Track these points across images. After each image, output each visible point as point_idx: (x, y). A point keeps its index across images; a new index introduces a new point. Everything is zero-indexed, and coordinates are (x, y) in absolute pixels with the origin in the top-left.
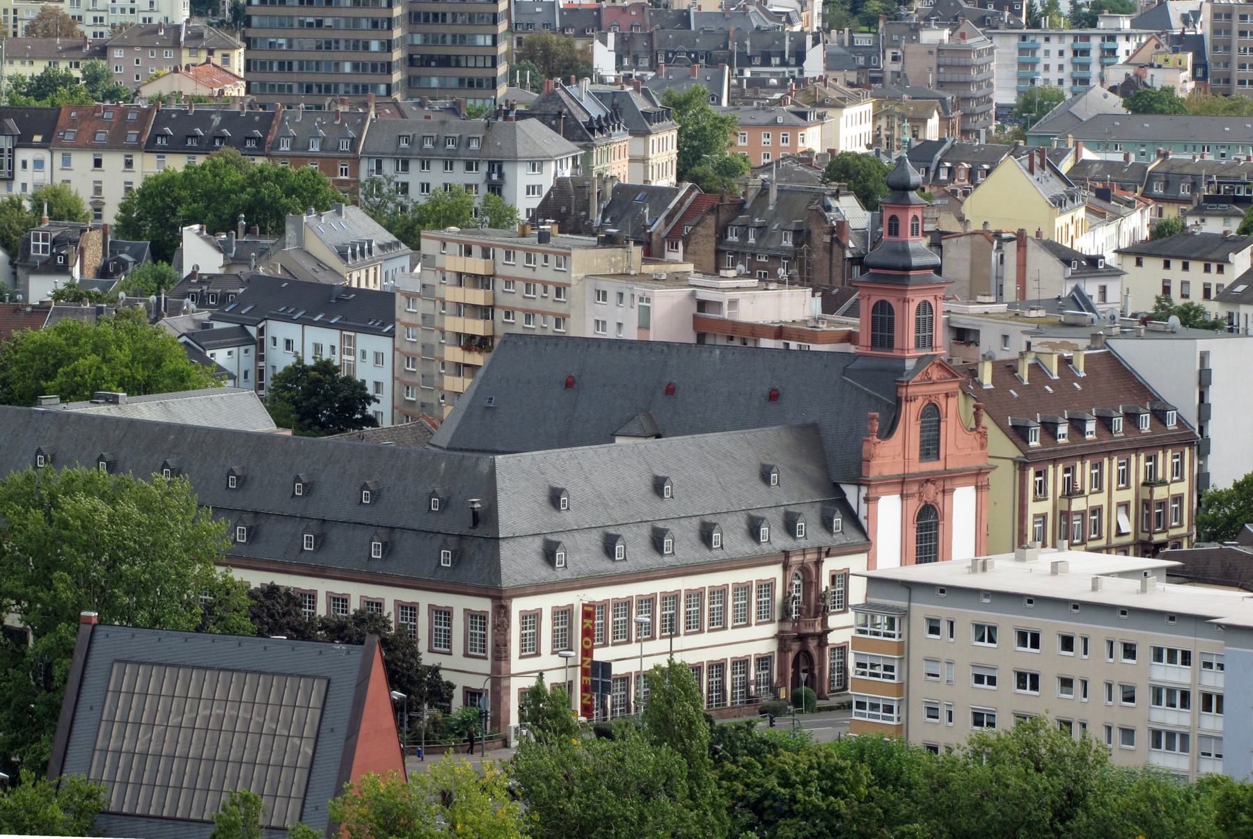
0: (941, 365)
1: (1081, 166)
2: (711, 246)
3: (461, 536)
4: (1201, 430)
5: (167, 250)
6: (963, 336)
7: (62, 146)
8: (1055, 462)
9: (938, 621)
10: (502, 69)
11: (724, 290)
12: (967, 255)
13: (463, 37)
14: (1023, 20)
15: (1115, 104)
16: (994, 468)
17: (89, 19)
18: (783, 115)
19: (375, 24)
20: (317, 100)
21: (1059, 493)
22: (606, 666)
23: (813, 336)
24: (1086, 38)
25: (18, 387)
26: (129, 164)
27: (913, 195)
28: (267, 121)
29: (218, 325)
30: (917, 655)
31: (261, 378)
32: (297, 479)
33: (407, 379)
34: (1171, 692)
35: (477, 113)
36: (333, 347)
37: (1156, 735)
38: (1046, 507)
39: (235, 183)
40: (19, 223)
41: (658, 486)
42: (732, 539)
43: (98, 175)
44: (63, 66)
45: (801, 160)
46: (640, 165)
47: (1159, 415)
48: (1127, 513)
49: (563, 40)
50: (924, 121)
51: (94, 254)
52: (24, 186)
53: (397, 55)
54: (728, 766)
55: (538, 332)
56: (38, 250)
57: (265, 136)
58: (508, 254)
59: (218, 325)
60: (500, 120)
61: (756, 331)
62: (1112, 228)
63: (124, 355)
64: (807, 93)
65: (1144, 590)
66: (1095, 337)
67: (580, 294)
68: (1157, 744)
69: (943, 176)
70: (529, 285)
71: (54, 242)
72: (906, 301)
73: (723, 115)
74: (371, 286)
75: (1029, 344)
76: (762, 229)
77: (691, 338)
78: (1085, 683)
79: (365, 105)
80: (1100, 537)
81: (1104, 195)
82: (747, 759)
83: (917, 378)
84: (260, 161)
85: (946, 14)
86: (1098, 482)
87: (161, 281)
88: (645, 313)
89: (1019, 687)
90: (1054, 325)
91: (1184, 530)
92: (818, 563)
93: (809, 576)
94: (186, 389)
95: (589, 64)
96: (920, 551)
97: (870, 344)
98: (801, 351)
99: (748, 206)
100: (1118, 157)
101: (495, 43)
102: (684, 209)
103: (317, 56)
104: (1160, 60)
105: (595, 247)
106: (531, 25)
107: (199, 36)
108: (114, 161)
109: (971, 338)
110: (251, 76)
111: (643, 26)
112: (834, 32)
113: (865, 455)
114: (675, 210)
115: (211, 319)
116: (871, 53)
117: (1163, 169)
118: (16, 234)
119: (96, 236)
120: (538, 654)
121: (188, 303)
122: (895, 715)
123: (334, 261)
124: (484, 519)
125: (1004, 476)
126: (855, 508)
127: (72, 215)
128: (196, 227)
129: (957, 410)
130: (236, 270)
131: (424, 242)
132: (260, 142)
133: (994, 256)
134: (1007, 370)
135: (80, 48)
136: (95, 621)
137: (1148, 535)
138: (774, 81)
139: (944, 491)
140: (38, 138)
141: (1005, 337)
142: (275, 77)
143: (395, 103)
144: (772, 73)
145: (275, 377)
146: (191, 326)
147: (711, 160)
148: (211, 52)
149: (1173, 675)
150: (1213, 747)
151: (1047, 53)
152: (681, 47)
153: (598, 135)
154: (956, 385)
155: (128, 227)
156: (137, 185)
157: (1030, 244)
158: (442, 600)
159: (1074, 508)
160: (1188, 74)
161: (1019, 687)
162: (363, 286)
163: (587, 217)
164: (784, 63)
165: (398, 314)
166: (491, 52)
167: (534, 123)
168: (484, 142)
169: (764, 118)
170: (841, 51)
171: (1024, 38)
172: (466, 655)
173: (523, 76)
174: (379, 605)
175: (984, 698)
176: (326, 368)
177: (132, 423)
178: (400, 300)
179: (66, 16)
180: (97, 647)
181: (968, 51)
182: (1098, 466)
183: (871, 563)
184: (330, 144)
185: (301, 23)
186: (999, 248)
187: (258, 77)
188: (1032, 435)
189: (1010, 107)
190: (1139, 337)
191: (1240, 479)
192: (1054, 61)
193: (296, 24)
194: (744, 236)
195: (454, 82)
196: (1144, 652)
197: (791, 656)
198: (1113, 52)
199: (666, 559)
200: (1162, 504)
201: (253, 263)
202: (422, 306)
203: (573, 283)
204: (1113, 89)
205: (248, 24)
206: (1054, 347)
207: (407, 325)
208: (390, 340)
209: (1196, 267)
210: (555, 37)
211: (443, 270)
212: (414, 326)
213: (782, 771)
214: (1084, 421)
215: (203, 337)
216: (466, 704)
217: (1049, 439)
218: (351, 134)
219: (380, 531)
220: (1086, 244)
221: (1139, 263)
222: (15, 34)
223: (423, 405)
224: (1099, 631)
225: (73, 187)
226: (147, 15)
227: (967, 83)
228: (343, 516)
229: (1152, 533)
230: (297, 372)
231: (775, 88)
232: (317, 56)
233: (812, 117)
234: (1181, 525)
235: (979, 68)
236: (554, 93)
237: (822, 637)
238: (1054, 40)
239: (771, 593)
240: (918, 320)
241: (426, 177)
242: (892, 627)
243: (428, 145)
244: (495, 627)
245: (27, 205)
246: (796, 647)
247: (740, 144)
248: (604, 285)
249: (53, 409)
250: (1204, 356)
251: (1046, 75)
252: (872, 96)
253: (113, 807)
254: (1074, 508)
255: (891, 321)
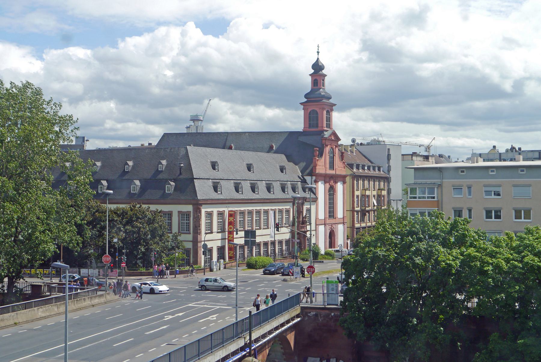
48: (375, 199)
97: (308, 127)
137: (380, 207)
244: (194, 218)
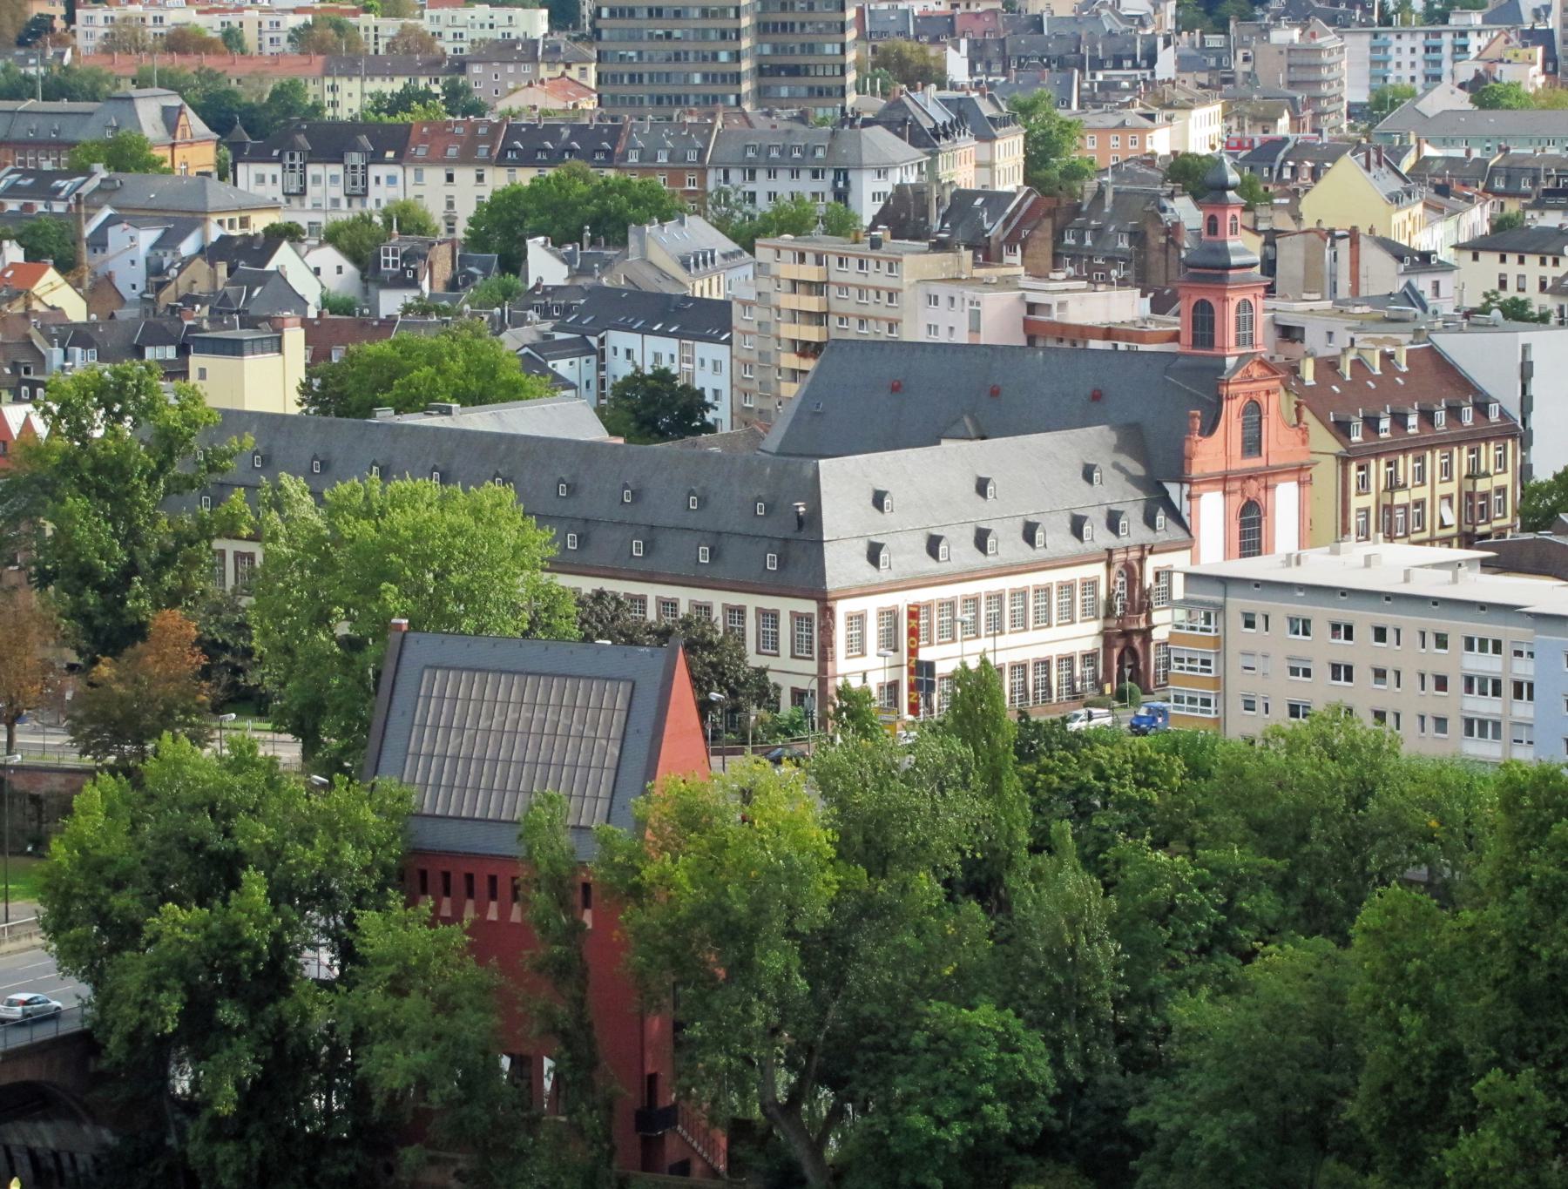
0: (1262, 363)
1: (1423, 163)
2: (1047, 248)
3: (786, 540)
4: (1524, 422)
5: (514, 262)
6: (1289, 333)
7: (413, 161)
8: (1377, 456)
9: (1253, 615)
10: (851, 77)
11: (1053, 292)
12: (1300, 252)
13: (811, 46)
14: (1376, 18)
15: (1462, 100)
16: (1316, 464)
17: (448, 34)
18: (1132, 116)
19: (723, 35)
20: (667, 112)
21: (1382, 486)
22: (930, 666)
23: (1141, 337)
24: (1438, 34)
25: (354, 400)
26: (480, 178)
27: (1231, 194)
28: (615, 133)
29: (559, 336)
30: (1233, 649)
31: (603, 387)
32: (626, 486)
33: (746, 386)
34: (1483, 681)
35: (823, 122)
36: (672, 356)
37: (1469, 723)
38: (1369, 501)
39: (581, 195)
40: (371, 238)
41: (982, 487)
42: (1056, 539)
43: (450, 190)
44: (422, 82)
45: (1144, 162)
46: (987, 170)
47: (1482, 408)
48: (1451, 505)
49: (916, 46)
50: (1275, 121)
51: (443, 267)
52: (378, 202)
53: (746, 65)
54: (1044, 760)
55: (872, 338)
56: (389, 262)
57: (614, 148)
58: (890, 266)
59: (559, 336)
60: (846, 128)
61: (1086, 332)
62: (1452, 222)
63: (458, 366)
64: (1156, 95)
65: (1455, 580)
66: (1417, 332)
67: (911, 298)
68: (1470, 732)
69: (1287, 175)
70: (862, 290)
71: (404, 257)
72: (1225, 300)
73: (1069, 119)
74: (715, 296)
75: (1352, 340)
76: (1099, 232)
77: (1022, 341)
78: (1398, 673)
79: (713, 115)
80: (1423, 530)
81: (1443, 190)
82: (1063, 753)
83: (1238, 376)
84: (611, 173)
85: (1298, 13)
86: (1421, 475)
87: (508, 293)
88: (975, 318)
89: (1334, 678)
90: (1378, 321)
91: (1508, 521)
92: (1141, 560)
93: (1132, 574)
94: (520, 399)
95: (943, 72)
96: (1243, 546)
98: (1129, 351)
99: (1085, 208)
100: (1461, 153)
101: (843, 51)
102: (1022, 213)
103: (667, 68)
104: (1509, 55)
105: (926, 252)
106: (885, 33)
107: (556, 50)
108: (465, 175)
109: (1297, 335)
110: (603, 88)
111: (996, 31)
112: (1185, 34)
113: (1186, 453)
114: (1013, 213)
115: (553, 329)
116: (1221, 54)
117: (1503, 164)
118: (368, 249)
119: (445, 250)
120: (863, 654)
121: (532, 315)
122: (1212, 708)
123: (679, 273)
124: (809, 527)
125: (1326, 472)
126: (1178, 505)
127: (421, 230)
128: (541, 239)
129: (1277, 406)
130: (581, 282)
131: (758, 250)
132: (609, 154)
133: (1328, 253)
134: (1329, 366)
135: (438, 63)
136: (405, 628)
138: (1125, 84)
139: (1266, 488)
140: (390, 154)
141: (1330, 334)
142: (626, 89)
143: (744, 114)
144: (1123, 76)
145: (614, 387)
146: (535, 338)
147: (1058, 163)
148: (568, 66)
149: (1485, 664)
150: (1524, 733)
151: (1399, 50)
152: (1034, 52)
153: (943, 141)
154: (1277, 383)
155: (477, 241)
156: (487, 199)
157: (1362, 240)
158: (769, 602)
159: (1396, 502)
160: (1538, 68)
161: (1334, 678)
162: (706, 296)
163: (926, 222)
164: (1136, 66)
165: (735, 322)
166: (840, 60)
167: (878, 130)
168: (830, 150)
169: (1112, 121)
170: (1193, 53)
171: (1376, 35)
172: (793, 656)
173: (873, 83)
174: (707, 609)
175: (1300, 690)
176: (663, 376)
177: (464, 434)
178: (736, 308)
179: (426, 32)
180: (407, 654)
181: (1318, 50)
182: (1422, 459)
183: (1195, 559)
184: (678, 154)
185: (651, 35)
186: (1333, 245)
187: (608, 91)
188: (1354, 431)
189: (1363, 105)
190: (1461, 331)
191: (1560, 470)
192: (1406, 58)
193: (646, 37)
194: (1081, 239)
195: (803, 91)
196: (1457, 642)
197: (1116, 652)
198: (1464, 48)
199: (989, 558)
200: (1485, 496)
201: (597, 274)
202: (758, 314)
203: (905, 288)
204: (1462, 86)
205: (599, 38)
206: (1377, 342)
207: (745, 333)
208: (726, 348)
209: (1532, 261)
210: (908, 45)
211: (777, 278)
212: (750, 333)
213: (1098, 765)
214: (1406, 416)
215: (547, 347)
216: (793, 703)
217: (1371, 434)
218: (699, 144)
219: (776, 543)
220: (1423, 241)
221: (1475, 258)
222: (376, 51)
223: (761, 412)
224: (1411, 622)
225: (426, 201)
226: (506, 30)
227: (1318, 83)
228: (670, 522)
229: (1475, 524)
230: (636, 381)
231: (1127, 91)
232: (667, 68)
233: (1160, 119)
234: (1505, 516)
235: (1330, 67)
236: (899, 100)
237: (1146, 635)
238: (1406, 37)
239: (1095, 592)
240: (1238, 319)
241: (772, 185)
242: (1208, 622)
243: (774, 154)
245: (377, 219)
246: (1120, 643)
247: (1089, 147)
248: (935, 289)
249: (387, 421)
250: (1526, 349)
251: (1399, 73)
252: (1222, 97)
253: (427, 810)
254: (1396, 502)
255: (1212, 320)
